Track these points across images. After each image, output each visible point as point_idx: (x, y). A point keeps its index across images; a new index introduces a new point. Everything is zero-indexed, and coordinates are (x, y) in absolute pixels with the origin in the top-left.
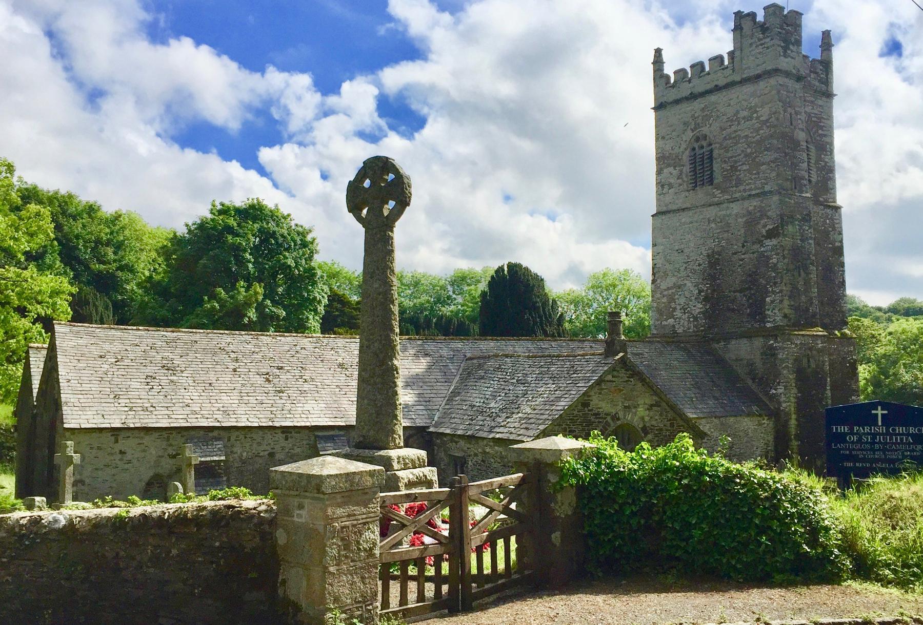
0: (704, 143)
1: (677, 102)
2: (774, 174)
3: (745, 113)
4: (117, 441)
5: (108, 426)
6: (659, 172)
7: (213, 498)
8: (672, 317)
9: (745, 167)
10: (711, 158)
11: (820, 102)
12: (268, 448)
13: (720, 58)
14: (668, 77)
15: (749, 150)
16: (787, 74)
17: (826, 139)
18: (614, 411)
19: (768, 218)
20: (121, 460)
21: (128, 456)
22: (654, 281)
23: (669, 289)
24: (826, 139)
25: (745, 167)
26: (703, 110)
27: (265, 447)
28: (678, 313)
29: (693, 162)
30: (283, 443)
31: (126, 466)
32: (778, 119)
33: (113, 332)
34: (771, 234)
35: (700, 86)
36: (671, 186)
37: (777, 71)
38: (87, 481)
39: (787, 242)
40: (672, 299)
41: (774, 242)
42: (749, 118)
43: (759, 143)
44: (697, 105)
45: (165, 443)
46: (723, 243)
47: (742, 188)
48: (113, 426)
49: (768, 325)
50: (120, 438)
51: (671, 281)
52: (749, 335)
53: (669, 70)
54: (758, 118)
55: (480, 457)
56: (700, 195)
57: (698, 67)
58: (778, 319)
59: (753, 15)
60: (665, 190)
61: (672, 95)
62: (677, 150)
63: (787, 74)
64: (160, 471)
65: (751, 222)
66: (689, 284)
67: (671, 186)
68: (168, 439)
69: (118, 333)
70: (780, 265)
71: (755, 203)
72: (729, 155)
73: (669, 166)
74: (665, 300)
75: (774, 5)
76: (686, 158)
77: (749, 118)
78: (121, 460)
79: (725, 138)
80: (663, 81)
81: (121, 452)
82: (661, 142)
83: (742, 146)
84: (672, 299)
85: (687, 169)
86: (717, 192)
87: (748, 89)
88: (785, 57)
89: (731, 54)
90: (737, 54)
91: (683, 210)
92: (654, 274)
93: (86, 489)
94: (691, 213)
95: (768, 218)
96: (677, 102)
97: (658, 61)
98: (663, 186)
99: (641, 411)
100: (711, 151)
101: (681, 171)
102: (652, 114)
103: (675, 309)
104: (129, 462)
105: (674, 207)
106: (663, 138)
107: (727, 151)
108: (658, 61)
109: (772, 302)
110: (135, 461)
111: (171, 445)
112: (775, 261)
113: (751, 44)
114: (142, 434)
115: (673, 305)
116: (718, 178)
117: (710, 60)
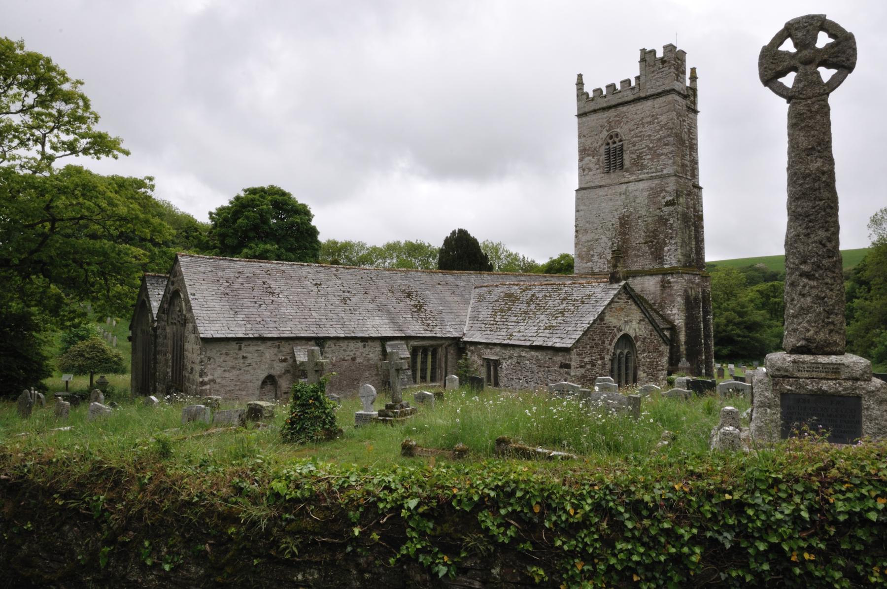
0: (617, 140)
1: (595, 111)
2: (671, 161)
3: (649, 119)
4: (240, 349)
5: (234, 336)
6: (581, 160)
7: (835, 371)
8: (591, 261)
9: (648, 157)
10: (622, 150)
11: (690, 116)
12: (351, 353)
13: (629, 81)
14: (587, 94)
15: (651, 145)
16: (679, 93)
17: (694, 141)
18: (618, 325)
19: (666, 192)
20: (244, 363)
21: (249, 361)
22: (576, 237)
23: (588, 241)
24: (694, 141)
25: (648, 157)
26: (616, 116)
27: (348, 353)
28: (596, 258)
29: (608, 152)
30: (361, 350)
31: (247, 368)
32: (674, 124)
33: (222, 262)
34: (668, 204)
35: (614, 100)
36: (590, 170)
37: (672, 91)
38: (218, 380)
39: (680, 209)
40: (590, 249)
41: (671, 208)
42: (650, 123)
43: (659, 140)
44: (612, 113)
45: (276, 349)
46: (632, 210)
47: (645, 171)
48: (238, 336)
49: (666, 266)
50: (243, 345)
51: (589, 236)
52: (651, 273)
53: (589, 89)
54: (658, 123)
55: (515, 360)
56: (614, 177)
57: (611, 87)
58: (673, 262)
59: (653, 52)
60: (586, 172)
61: (592, 106)
62: (595, 145)
63: (679, 93)
64: (273, 372)
65: (654, 194)
66: (604, 238)
67: (590, 170)
68: (279, 347)
69: (226, 263)
70: (675, 225)
71: (657, 182)
72: (636, 148)
73: (589, 155)
74: (585, 249)
75: (671, 45)
76: (603, 150)
77: (650, 123)
78: (244, 363)
79: (632, 137)
80: (585, 97)
81: (244, 357)
82: (583, 140)
83: (646, 142)
84: (590, 249)
85: (603, 157)
86: (626, 174)
87: (649, 103)
88: (677, 80)
89: (638, 78)
90: (642, 78)
91: (600, 187)
92: (577, 231)
93: (217, 387)
94: (606, 188)
95: (666, 192)
96: (595, 111)
97: (580, 83)
98: (584, 170)
99: (635, 324)
100: (622, 145)
101: (598, 160)
102: (576, 119)
103: (593, 256)
104: (250, 365)
105: (593, 185)
106: (584, 136)
107: (634, 146)
108: (580, 83)
109: (669, 250)
110: (254, 364)
111: (281, 351)
112: (671, 222)
113: (653, 72)
114: (259, 343)
115: (592, 253)
116: (627, 163)
117: (622, 82)
